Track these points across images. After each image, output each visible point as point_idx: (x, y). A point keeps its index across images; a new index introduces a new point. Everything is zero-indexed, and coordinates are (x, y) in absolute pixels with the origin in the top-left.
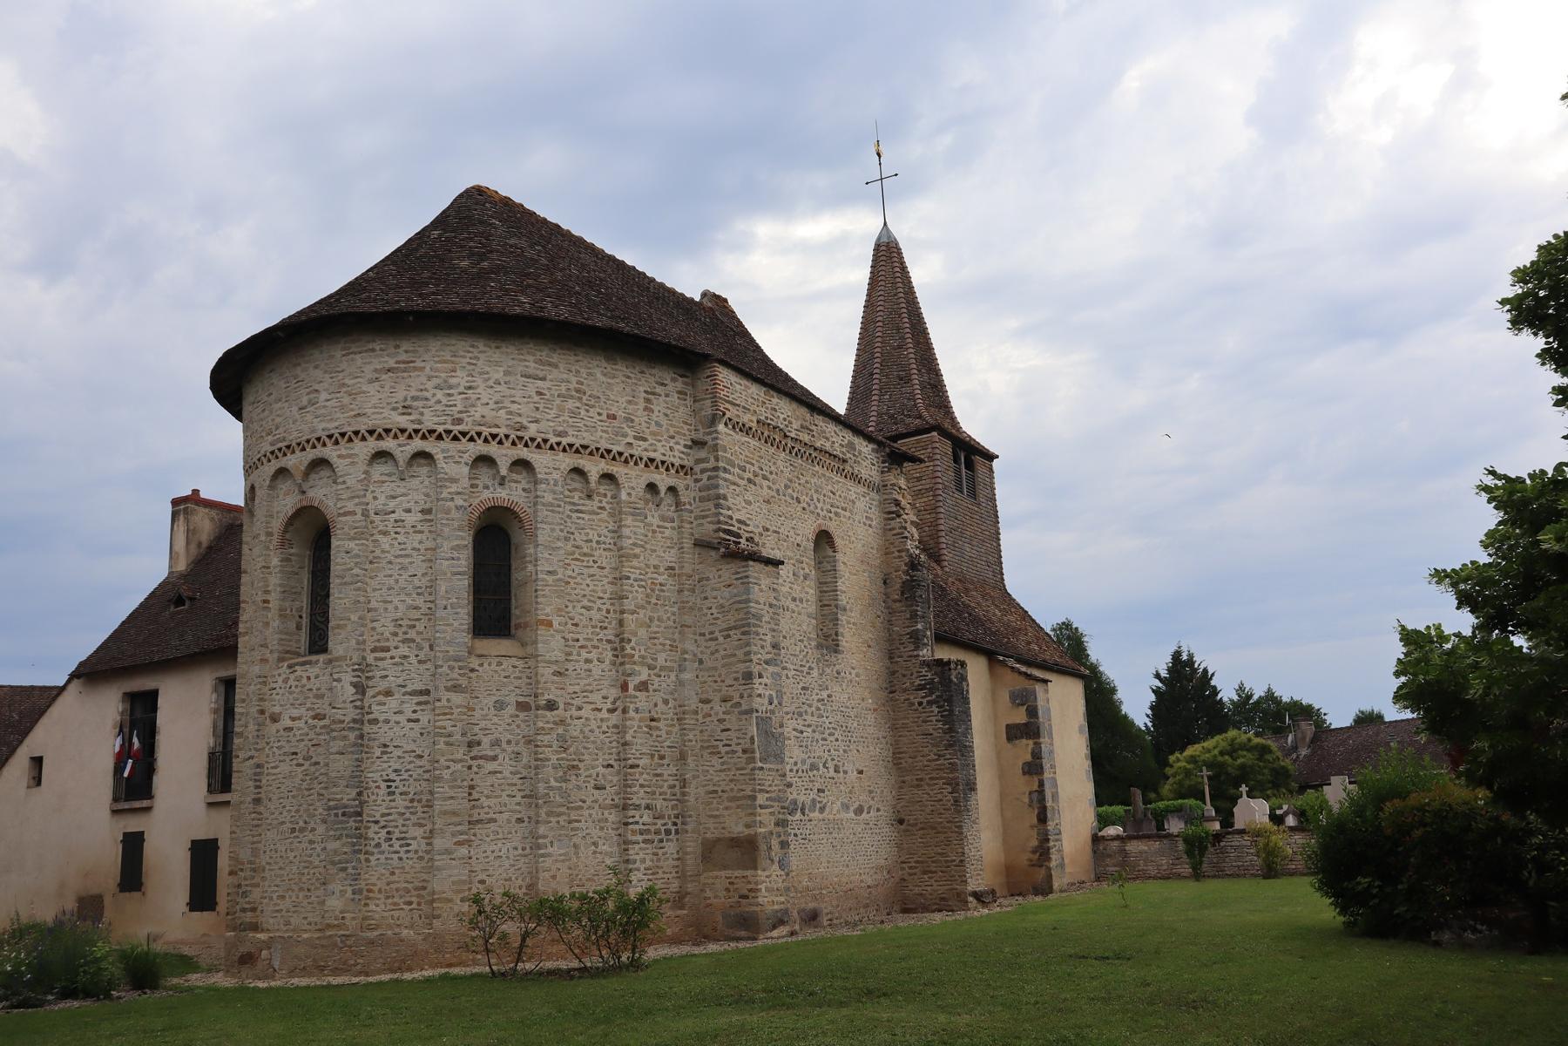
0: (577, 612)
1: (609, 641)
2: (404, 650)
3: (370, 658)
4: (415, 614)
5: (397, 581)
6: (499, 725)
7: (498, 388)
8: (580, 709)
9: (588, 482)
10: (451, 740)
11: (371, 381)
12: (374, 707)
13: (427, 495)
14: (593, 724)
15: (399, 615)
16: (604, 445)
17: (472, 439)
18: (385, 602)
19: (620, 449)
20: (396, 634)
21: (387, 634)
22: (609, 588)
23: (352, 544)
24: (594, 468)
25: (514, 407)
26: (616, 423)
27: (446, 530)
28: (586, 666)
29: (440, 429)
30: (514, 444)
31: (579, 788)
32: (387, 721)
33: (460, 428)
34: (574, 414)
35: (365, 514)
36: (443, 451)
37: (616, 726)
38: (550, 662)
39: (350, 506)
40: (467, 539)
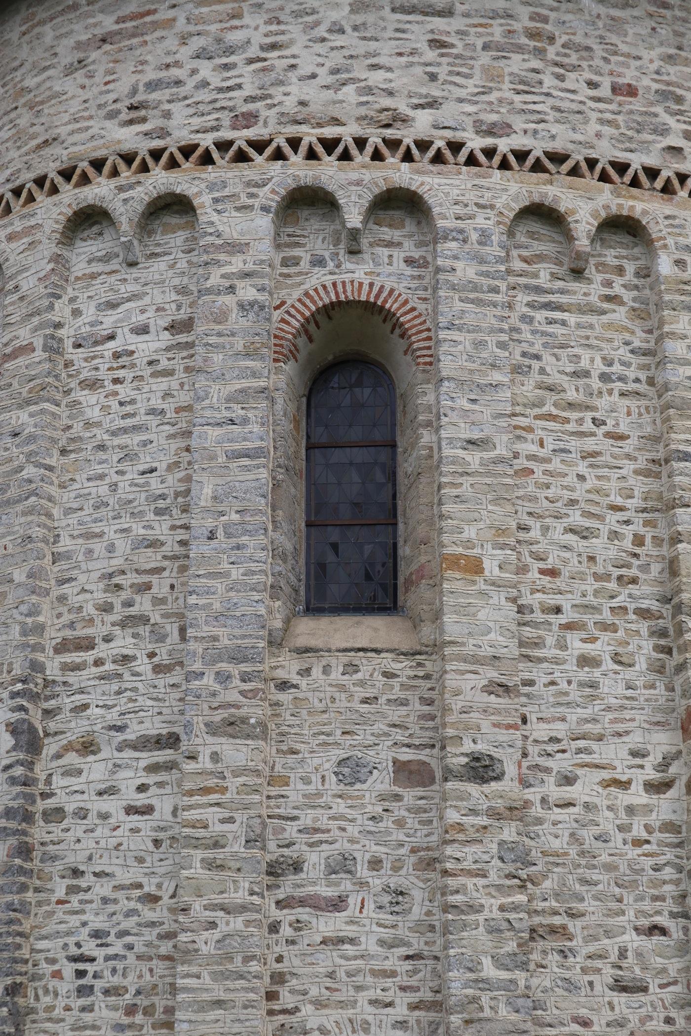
0: (553, 541)
1: (644, 614)
2: (124, 643)
3: (53, 669)
4: (149, 559)
5: (114, 487)
6: (350, 821)
7: (339, 40)
8: (568, 780)
9: (569, 237)
10: (219, 854)
11: (69, 71)
12: (58, 781)
13: (183, 291)
14: (607, 822)
15: (117, 562)
16: (606, 152)
17: (279, 155)
18: (89, 536)
19: (652, 161)
20: (107, 608)
21: (90, 609)
22: (640, 486)
23: (23, 416)
24: (585, 205)
25: (377, 78)
26: (636, 104)
27: (217, 358)
28: (584, 674)
29: (207, 141)
30: (377, 156)
31: (570, 986)
32: (82, 814)
33: (251, 133)
34: (525, 85)
35: (54, 348)
36: (212, 187)
37: (670, 827)
38: (476, 660)
39: (24, 335)
40: (281, 379)
